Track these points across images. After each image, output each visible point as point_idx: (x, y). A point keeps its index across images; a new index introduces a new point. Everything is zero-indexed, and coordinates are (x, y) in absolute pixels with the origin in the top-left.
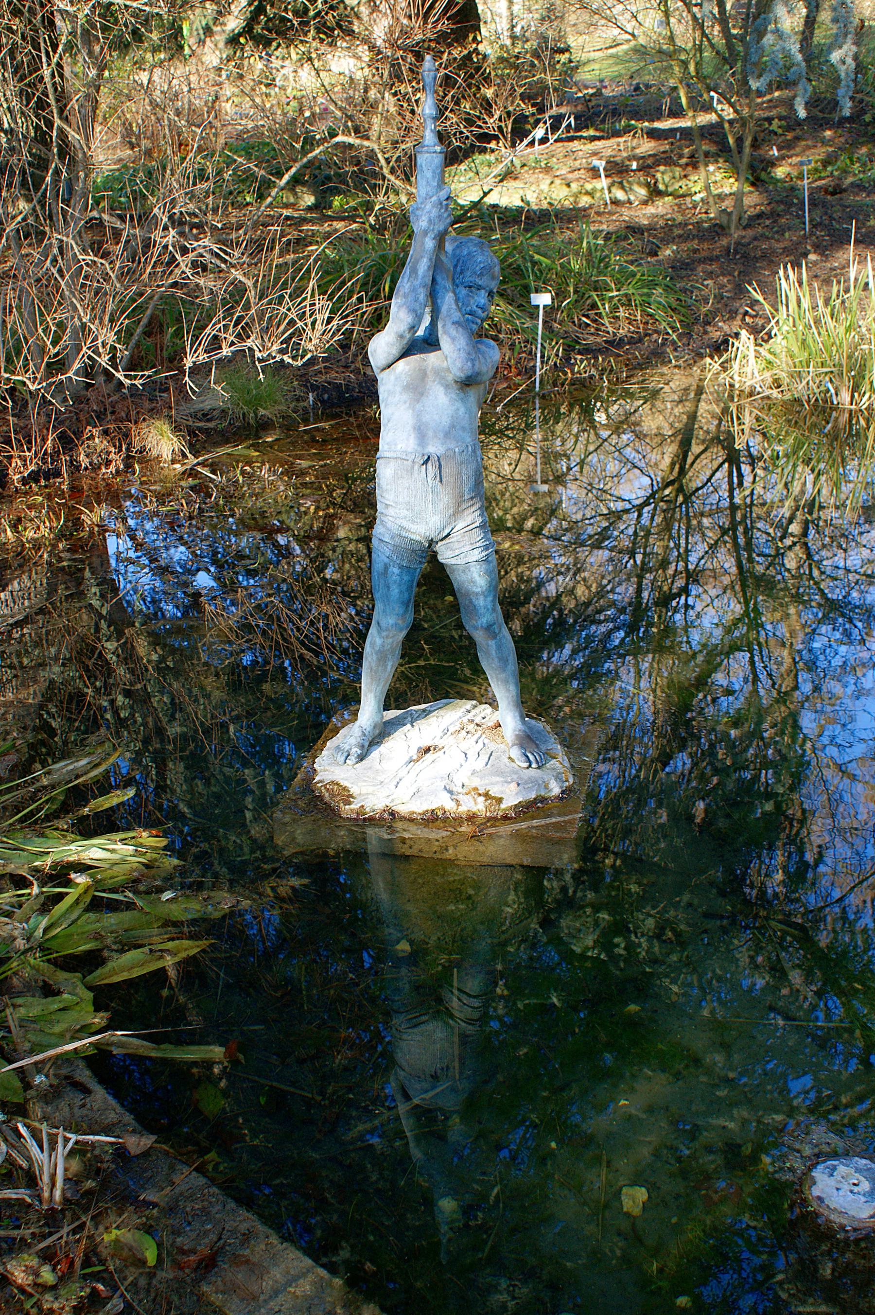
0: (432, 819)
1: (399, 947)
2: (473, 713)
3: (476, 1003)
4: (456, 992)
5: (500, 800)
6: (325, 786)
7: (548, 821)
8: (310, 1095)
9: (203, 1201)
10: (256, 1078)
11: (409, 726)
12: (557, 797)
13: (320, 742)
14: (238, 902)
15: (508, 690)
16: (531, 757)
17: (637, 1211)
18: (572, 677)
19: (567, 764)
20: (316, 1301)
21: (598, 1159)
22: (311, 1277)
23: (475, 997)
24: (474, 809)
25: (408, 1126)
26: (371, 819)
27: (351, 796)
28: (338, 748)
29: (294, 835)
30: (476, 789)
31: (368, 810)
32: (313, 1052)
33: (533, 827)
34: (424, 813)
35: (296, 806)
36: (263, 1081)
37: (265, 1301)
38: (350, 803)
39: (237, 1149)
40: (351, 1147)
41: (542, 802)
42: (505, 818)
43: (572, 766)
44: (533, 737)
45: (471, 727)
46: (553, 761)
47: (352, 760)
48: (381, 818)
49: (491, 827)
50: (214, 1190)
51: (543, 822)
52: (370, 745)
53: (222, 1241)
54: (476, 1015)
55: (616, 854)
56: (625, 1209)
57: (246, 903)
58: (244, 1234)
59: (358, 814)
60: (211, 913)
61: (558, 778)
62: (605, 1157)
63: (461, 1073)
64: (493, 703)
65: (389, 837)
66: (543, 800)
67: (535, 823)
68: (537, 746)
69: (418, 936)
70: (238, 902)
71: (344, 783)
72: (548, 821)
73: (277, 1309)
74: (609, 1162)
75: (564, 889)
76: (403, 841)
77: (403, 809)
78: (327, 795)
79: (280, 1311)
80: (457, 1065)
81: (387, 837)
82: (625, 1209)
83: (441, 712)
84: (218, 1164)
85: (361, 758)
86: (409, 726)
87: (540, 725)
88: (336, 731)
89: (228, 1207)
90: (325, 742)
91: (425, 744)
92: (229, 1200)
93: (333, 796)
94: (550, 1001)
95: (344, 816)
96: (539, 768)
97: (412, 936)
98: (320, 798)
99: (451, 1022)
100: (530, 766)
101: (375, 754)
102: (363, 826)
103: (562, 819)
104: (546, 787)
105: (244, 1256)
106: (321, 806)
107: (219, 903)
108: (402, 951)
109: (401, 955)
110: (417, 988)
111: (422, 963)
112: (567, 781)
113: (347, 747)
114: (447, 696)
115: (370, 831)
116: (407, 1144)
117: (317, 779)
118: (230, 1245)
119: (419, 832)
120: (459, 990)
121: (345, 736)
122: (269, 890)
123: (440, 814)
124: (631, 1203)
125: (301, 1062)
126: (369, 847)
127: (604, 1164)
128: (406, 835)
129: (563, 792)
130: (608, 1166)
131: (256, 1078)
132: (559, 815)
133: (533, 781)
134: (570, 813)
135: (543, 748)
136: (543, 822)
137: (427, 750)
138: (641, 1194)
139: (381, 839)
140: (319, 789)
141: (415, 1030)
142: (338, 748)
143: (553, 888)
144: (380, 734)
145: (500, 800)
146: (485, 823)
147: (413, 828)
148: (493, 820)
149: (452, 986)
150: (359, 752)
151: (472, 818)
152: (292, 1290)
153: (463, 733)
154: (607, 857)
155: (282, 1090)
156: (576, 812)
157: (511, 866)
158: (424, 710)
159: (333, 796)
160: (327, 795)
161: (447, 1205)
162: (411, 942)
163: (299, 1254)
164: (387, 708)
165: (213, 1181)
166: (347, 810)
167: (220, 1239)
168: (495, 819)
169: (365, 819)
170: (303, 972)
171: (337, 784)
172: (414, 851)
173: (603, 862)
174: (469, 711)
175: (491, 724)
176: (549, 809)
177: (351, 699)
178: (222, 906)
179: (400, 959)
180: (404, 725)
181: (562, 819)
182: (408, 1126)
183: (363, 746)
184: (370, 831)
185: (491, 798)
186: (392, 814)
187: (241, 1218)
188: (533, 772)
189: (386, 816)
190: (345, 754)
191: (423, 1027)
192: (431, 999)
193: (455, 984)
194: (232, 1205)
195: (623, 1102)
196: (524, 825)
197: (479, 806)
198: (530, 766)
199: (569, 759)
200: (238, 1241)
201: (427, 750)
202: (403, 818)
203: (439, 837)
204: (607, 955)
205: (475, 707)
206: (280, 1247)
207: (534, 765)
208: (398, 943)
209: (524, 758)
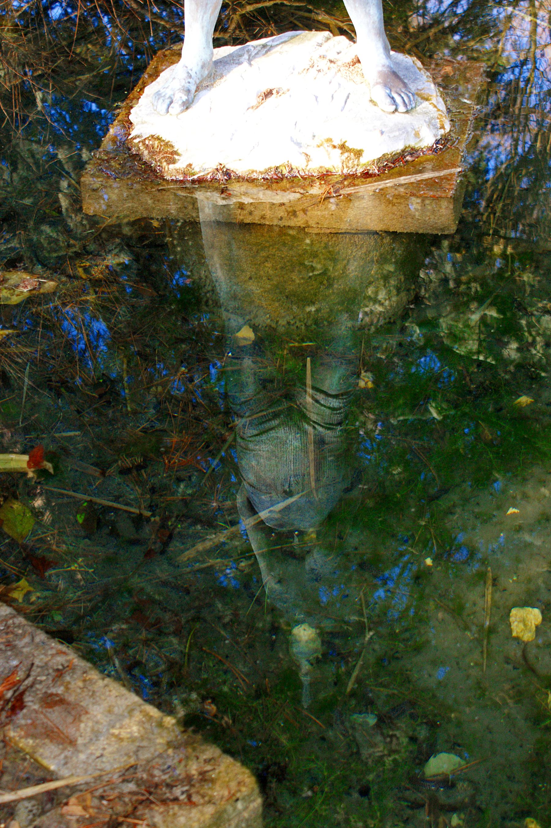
0: (276, 180)
1: (240, 334)
2: (326, 45)
3: (335, 403)
4: (310, 390)
5: (359, 153)
6: (143, 142)
7: (419, 177)
8: (137, 511)
9: (7, 633)
10: (71, 493)
11: (245, 64)
12: (431, 149)
13: (137, 89)
14: (40, 283)
15: (368, 14)
16: (398, 100)
17: (528, 636)
18: (453, 30)
19: (442, 107)
20: (145, 743)
21: (481, 576)
22: (138, 716)
23: (336, 396)
24: (328, 165)
25: (256, 544)
26: (200, 181)
27: (176, 153)
28: (158, 95)
29: (108, 198)
30: (329, 140)
31: (197, 169)
32: (139, 460)
33: (401, 185)
34: (266, 172)
35: (109, 168)
36: (79, 496)
37: (85, 745)
38: (174, 162)
39: (50, 576)
40: (188, 569)
41: (411, 154)
42: (367, 175)
43: (449, 111)
44: (401, 74)
45: (323, 64)
46: (426, 104)
47: (176, 107)
48: (213, 179)
49: (348, 186)
50: (20, 620)
51: (413, 178)
52: (198, 90)
53: (31, 679)
54: (336, 418)
55: (508, 240)
56: (514, 634)
57: (50, 285)
58: (58, 670)
59: (185, 174)
60: (7, 299)
61: (430, 124)
62: (490, 575)
63: (317, 480)
64: (348, 32)
65: (224, 202)
66: (413, 151)
67: (403, 180)
68: (405, 85)
69: (263, 320)
70: (40, 283)
71: (165, 137)
72: (419, 177)
73: (98, 754)
74: (494, 580)
75: (445, 281)
76: (241, 206)
77: (240, 168)
78: (146, 153)
79: (102, 755)
80: (312, 472)
81: (221, 202)
82: (514, 634)
83: (285, 47)
84: (28, 594)
85: (187, 105)
86: (245, 64)
87: (407, 60)
88: (155, 75)
89: (37, 639)
90: (142, 90)
91: (265, 88)
92: (39, 631)
93: (152, 153)
94: (428, 416)
95: (168, 178)
96: (407, 112)
97: (257, 321)
98: (137, 157)
99: (306, 426)
100: (396, 110)
101: (206, 98)
102: (191, 191)
103: (436, 174)
104: (417, 135)
105: (57, 695)
106: (140, 167)
107: (17, 286)
108: (245, 339)
109: (243, 343)
110: (265, 383)
111: (268, 353)
112: (442, 127)
113: (169, 93)
114: (294, 28)
115: (200, 195)
116: (256, 562)
117: (133, 133)
118: (41, 682)
119: (261, 195)
120: (314, 388)
121: (167, 81)
122: (80, 270)
123: (285, 172)
124: (521, 626)
125: (125, 472)
126: (201, 215)
127: (490, 582)
128: (246, 200)
129: (437, 142)
130: (494, 585)
131: (71, 493)
132: (433, 170)
133: (403, 129)
134: (447, 167)
135: (413, 87)
136: (413, 178)
137: (269, 94)
138: (534, 615)
139: (215, 206)
140: (137, 145)
141: (264, 437)
142: (158, 95)
143: (431, 281)
144: (209, 76)
145: (359, 153)
146: (342, 182)
147: (252, 190)
148: (351, 178)
149: (305, 384)
150: (185, 98)
151: (325, 176)
152: (116, 732)
153: (313, 71)
154: (497, 243)
155: (70, 436)
156: (454, 166)
157: (376, 233)
158: (264, 46)
159: (152, 153)
160: (146, 153)
161: (304, 634)
162: (255, 328)
163: (123, 691)
164: (217, 43)
165: (19, 611)
166: (171, 171)
167: (28, 676)
168: (354, 176)
169: (193, 182)
170: (125, 366)
171: (158, 139)
172: (255, 218)
173: (491, 250)
174: (320, 45)
175: (349, 60)
176: (421, 163)
177: (173, 37)
178: (21, 289)
179: (242, 349)
180: (240, 64)
181: (436, 174)
182: (256, 544)
183: (189, 91)
184: (200, 195)
185: (350, 151)
186: (227, 173)
187: (54, 651)
188: (401, 118)
189: (219, 176)
190: (168, 101)
191: (272, 434)
192: (281, 400)
193: (309, 382)
194: (41, 636)
195: (511, 510)
196: (389, 183)
197: (335, 163)
198: (396, 110)
199: (445, 102)
200: (51, 678)
201: (269, 94)
202: (240, 179)
203: (285, 200)
204: (495, 359)
205: (328, 39)
206: (101, 683)
207: (402, 108)
208: (239, 330)
209: (389, 100)
